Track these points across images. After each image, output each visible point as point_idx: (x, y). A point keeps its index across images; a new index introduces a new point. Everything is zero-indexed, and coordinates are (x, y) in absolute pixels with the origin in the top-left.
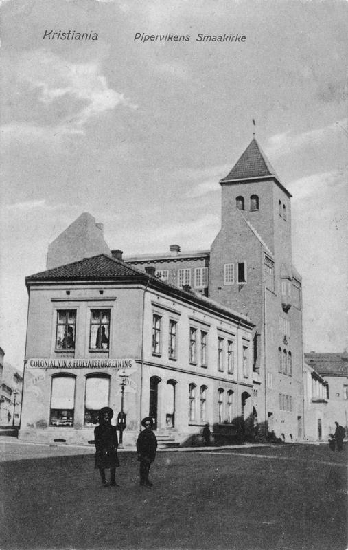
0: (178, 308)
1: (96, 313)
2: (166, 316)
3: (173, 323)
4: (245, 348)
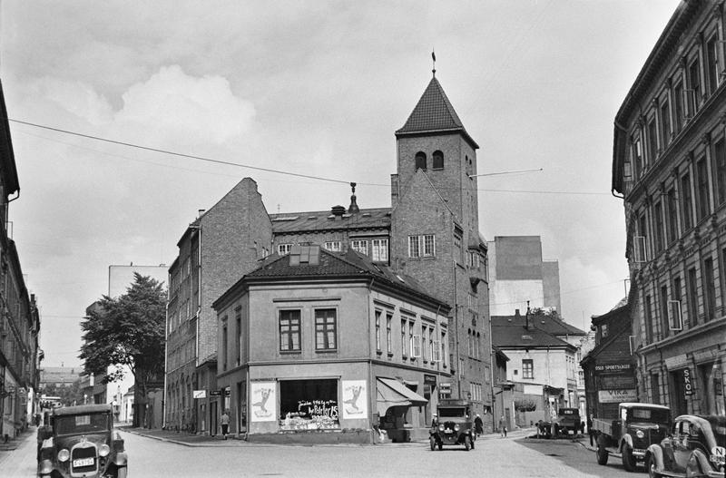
0: (392, 301)
1: (319, 313)
2: (384, 311)
3: (389, 317)
4: (443, 334)
